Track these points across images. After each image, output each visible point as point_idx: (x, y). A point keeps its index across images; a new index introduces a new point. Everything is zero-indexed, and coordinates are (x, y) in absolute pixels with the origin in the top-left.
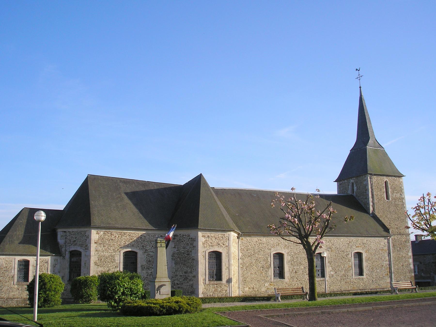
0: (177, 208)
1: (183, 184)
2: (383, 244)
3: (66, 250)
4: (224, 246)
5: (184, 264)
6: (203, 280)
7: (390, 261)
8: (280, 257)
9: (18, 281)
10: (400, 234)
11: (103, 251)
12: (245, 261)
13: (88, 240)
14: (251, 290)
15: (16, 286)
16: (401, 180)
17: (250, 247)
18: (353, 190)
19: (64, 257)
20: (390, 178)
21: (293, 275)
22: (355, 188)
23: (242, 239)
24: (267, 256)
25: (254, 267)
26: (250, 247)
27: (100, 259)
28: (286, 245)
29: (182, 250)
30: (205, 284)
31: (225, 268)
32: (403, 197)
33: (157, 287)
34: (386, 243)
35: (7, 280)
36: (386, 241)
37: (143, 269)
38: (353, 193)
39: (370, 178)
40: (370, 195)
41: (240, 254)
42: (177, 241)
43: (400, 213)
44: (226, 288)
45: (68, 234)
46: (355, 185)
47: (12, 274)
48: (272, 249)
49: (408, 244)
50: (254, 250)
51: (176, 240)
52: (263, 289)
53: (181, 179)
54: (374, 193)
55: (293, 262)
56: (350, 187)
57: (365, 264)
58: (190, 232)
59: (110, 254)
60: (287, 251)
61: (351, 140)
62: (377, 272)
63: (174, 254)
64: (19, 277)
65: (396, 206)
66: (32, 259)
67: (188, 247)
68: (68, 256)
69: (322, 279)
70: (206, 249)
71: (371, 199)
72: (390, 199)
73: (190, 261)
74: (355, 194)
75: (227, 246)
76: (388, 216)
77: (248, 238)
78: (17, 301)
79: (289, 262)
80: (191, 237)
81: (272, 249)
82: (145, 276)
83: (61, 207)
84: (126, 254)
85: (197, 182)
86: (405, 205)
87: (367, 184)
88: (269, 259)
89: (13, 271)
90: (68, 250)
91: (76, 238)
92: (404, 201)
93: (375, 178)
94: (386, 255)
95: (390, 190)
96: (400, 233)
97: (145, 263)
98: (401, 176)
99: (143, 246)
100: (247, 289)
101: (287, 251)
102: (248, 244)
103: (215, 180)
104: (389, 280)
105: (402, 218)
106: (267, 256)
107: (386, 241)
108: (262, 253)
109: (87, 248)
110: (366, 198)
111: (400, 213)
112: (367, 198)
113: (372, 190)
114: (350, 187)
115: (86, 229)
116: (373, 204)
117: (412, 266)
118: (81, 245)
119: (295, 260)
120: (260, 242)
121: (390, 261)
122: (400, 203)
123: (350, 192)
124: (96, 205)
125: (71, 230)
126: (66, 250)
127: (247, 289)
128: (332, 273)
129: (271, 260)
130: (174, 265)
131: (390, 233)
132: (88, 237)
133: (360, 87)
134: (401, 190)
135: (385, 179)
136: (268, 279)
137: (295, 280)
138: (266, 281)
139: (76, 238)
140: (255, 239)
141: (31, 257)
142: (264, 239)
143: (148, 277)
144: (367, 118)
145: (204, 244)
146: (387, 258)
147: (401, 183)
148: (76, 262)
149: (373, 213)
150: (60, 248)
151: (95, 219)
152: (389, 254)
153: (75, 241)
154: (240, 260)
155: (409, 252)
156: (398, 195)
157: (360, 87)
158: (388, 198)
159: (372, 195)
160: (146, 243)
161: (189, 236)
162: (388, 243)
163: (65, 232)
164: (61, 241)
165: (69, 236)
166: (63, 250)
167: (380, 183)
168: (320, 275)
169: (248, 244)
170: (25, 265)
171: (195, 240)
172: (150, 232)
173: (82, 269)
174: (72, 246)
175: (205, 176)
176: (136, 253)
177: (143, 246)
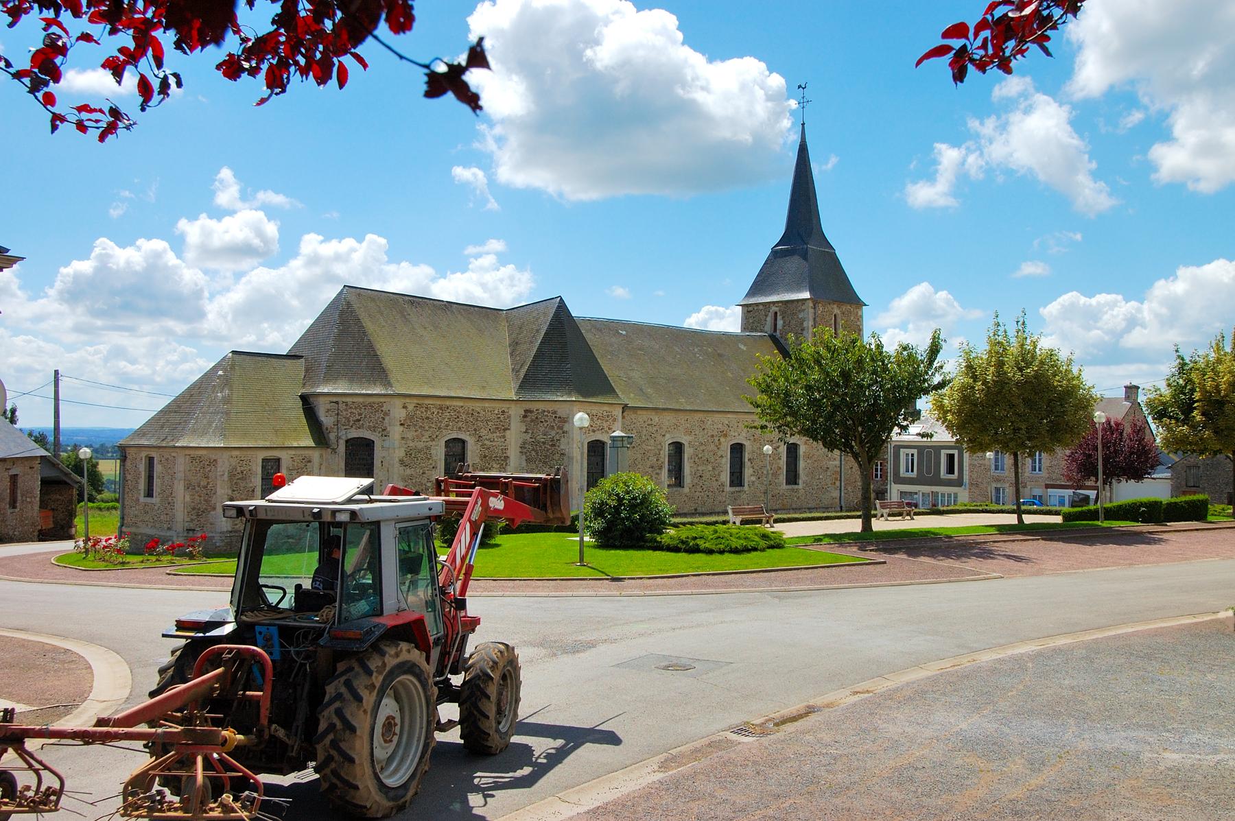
3: (338, 438)
5: (545, 463)
18: (775, 325)
22: (780, 323)
29: (541, 438)
38: (775, 330)
42: (532, 421)
45: (342, 407)
46: (779, 317)
57: (802, 464)
67: (553, 433)
68: (342, 448)
69: (737, 489)
73: (557, 457)
81: (668, 436)
90: (344, 438)
97: (477, 460)
103: (442, 280)
114: (769, 319)
118: (373, 429)
123: (409, 576)
126: (338, 438)
128: (753, 478)
129: (665, 452)
130: (524, 464)
160: (480, 424)
163: (337, 403)
166: (332, 436)
175: (423, 92)
176: (463, 442)
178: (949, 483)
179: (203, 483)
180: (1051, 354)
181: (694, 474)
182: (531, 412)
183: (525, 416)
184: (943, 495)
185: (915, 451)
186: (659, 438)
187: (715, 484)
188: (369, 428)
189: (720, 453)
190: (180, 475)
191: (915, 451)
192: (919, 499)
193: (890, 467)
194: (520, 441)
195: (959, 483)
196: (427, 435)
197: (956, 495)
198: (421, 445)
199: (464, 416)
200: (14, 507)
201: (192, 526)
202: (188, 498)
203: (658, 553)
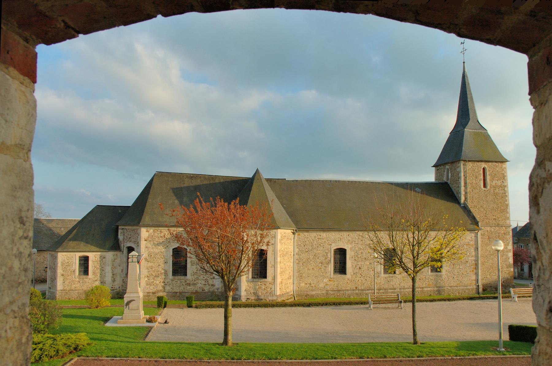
2: (470, 239)
7: (477, 256)
8: (341, 253)
9: (79, 274)
10: (498, 225)
12: (301, 257)
14: (308, 285)
15: (77, 279)
16: (504, 166)
17: (307, 242)
20: (490, 164)
22: (450, 175)
23: (299, 235)
24: (327, 251)
25: (312, 262)
27: (150, 255)
28: (349, 240)
31: (270, 266)
32: (505, 184)
33: (126, 302)
34: (473, 238)
35: (69, 274)
36: (473, 235)
37: (192, 265)
39: (464, 165)
40: (462, 184)
43: (501, 202)
44: (271, 286)
47: (73, 268)
48: (333, 245)
49: (508, 237)
50: (312, 246)
52: (321, 285)
54: (468, 181)
55: (356, 258)
56: (445, 173)
60: (350, 246)
61: (449, 121)
62: (459, 268)
64: (80, 271)
65: (495, 194)
71: (463, 188)
72: (488, 187)
74: (449, 182)
75: (273, 244)
76: (485, 206)
77: (306, 234)
78: (78, 293)
79: (352, 257)
81: (333, 245)
82: (195, 271)
86: (507, 194)
87: (459, 172)
88: (329, 254)
89: (74, 266)
92: (506, 189)
93: (470, 165)
94: (472, 250)
95: (488, 178)
96: (498, 224)
98: (504, 161)
101: (350, 246)
102: (306, 240)
104: (474, 277)
105: (502, 208)
107: (473, 235)
108: (322, 248)
110: (458, 187)
111: (501, 202)
112: (459, 187)
113: (465, 178)
114: (445, 173)
115: (137, 228)
116: (466, 193)
118: (135, 242)
119: (359, 256)
120: (320, 237)
121: (477, 256)
122: (501, 192)
123: (445, 179)
125: (127, 227)
131: (480, 226)
132: (139, 234)
133: (464, 63)
134: (503, 177)
135: (483, 165)
136: (328, 275)
137: (359, 275)
138: (324, 277)
140: (313, 235)
141: (91, 253)
142: (324, 235)
143: (198, 272)
144: (469, 96)
146: (473, 253)
147: (504, 169)
149: (464, 203)
152: (477, 249)
154: (296, 256)
155: (508, 245)
156: (499, 183)
157: (464, 63)
158: (485, 186)
159: (465, 183)
162: (476, 237)
164: (120, 237)
166: (122, 245)
167: (476, 170)
169: (306, 240)
174: (128, 243)
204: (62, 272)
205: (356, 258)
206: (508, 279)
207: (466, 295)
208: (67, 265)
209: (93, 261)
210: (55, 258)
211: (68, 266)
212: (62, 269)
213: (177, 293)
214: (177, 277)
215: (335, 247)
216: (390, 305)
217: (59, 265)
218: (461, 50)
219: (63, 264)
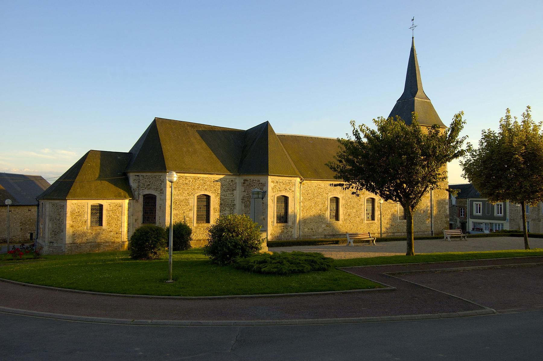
0: (247, 152)
1: (246, 129)
3: (139, 194)
4: (290, 191)
6: (272, 222)
11: (178, 195)
13: (163, 184)
19: (137, 201)
21: (346, 217)
24: (325, 200)
26: (310, 191)
30: (273, 225)
35: (79, 225)
37: (215, 212)
41: (302, 198)
42: (247, 185)
44: (291, 230)
45: (141, 178)
47: (85, 218)
50: (314, 194)
51: (246, 184)
52: (320, 230)
53: (244, 123)
55: (346, 206)
58: (261, 178)
59: (184, 198)
63: (244, 197)
66: (105, 203)
68: (141, 200)
69: (371, 222)
70: (274, 194)
75: (293, 191)
78: (91, 246)
80: (261, 182)
81: (330, 194)
83: (126, 148)
84: (199, 198)
85: (265, 128)
88: (326, 202)
91: (150, 182)
99: (215, 190)
100: (306, 230)
103: (280, 128)
106: (325, 200)
109: (163, 192)
115: (160, 174)
117: (448, 212)
118: (156, 189)
124: (169, 148)
125: (144, 174)
126: (139, 194)
127: (306, 230)
130: (243, 208)
133: (413, 38)
139: (150, 182)
140: (315, 183)
145: (273, 189)
148: (150, 206)
150: (133, 191)
151: (169, 163)
153: (149, 185)
157: (413, 38)
161: (259, 181)
163: (138, 176)
164: (133, 184)
165: (143, 180)
166: (136, 193)
168: (370, 218)
170: (98, 211)
171: (265, 185)
172: (228, 177)
173: (157, 212)
177: (215, 190)
178: (499, 219)
179: (58, 218)
180: (488, 137)
181: (345, 215)
182: (247, 180)
183: (244, 183)
184: (496, 225)
185: (481, 203)
186: (325, 195)
187: (358, 219)
188: (154, 189)
189: (360, 203)
190: (47, 213)
191: (481, 203)
192: (483, 226)
193: (468, 211)
194: (241, 196)
195: (504, 218)
196: (186, 193)
197: (502, 224)
198: (182, 198)
199: (208, 183)
200: (373, 219)
201: (52, 240)
202: (50, 226)
203: (477, 238)
204: (71, 223)
205: (346, 206)
206: (278, 236)
207: (428, 233)
208: (78, 215)
209: (107, 210)
210: (64, 207)
211: (79, 215)
212: (72, 219)
213: (201, 240)
214: (200, 225)
215: (331, 196)
216: (456, 239)
217: (68, 214)
218: (411, 26)
219: (72, 213)
